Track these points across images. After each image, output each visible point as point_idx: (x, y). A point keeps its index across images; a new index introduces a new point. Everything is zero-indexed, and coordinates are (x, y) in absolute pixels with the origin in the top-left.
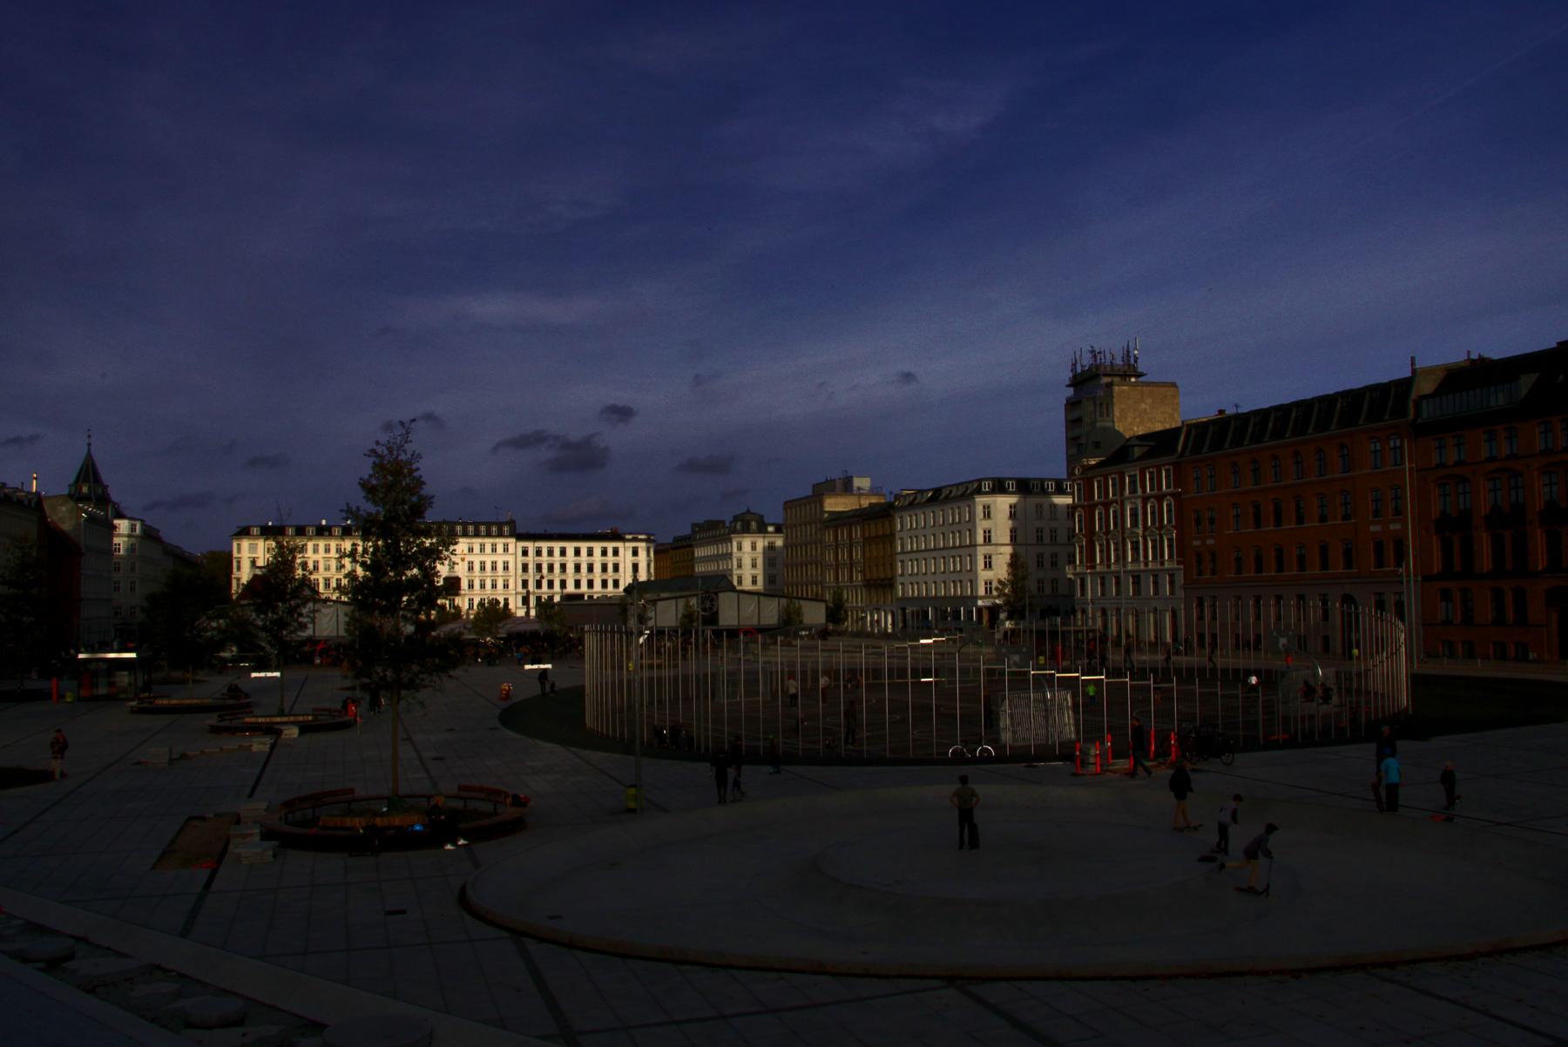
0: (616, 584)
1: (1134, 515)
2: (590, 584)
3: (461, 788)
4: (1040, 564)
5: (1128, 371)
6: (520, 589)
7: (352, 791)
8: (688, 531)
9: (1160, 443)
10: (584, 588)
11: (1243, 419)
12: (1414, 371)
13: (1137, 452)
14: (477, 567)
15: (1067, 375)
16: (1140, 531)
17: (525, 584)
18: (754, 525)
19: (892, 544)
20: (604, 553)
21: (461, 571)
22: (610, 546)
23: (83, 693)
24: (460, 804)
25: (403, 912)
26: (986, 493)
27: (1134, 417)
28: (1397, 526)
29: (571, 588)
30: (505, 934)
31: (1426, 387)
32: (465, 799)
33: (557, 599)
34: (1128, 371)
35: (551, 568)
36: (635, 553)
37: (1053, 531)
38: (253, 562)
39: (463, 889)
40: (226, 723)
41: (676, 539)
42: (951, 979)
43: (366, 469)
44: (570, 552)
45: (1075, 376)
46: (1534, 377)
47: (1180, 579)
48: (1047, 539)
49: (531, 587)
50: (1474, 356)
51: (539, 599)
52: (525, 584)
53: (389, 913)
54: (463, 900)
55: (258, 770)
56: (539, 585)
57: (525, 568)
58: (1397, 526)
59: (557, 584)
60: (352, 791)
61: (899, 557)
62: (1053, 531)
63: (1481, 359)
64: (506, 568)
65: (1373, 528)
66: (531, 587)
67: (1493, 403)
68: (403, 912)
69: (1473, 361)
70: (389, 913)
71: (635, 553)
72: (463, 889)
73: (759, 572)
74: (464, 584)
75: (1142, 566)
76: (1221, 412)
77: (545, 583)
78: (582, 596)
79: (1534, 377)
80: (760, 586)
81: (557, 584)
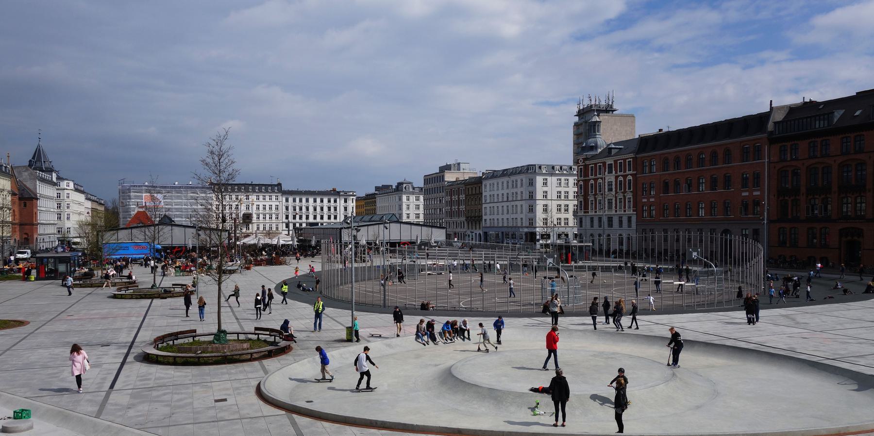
0: (335, 218)
2: (322, 218)
3: (256, 329)
4: (559, 210)
5: (608, 110)
6: (284, 220)
7: (195, 331)
8: (372, 191)
10: (318, 220)
11: (669, 135)
12: (771, 108)
14: (261, 208)
15: (575, 110)
19: (480, 199)
21: (253, 210)
24: (255, 337)
27: (609, 134)
28: (758, 193)
29: (311, 220)
31: (779, 117)
32: (258, 334)
34: (608, 110)
35: (301, 209)
40: (123, 292)
41: (367, 195)
43: (204, 155)
45: (579, 111)
46: (842, 112)
47: (634, 219)
49: (291, 219)
50: (807, 100)
51: (294, 225)
52: (287, 217)
53: (216, 401)
54: (260, 393)
55: (142, 319)
56: (294, 218)
58: (758, 193)
59: (304, 217)
60: (195, 331)
61: (484, 206)
63: (811, 102)
64: (277, 209)
65: (744, 194)
66: (291, 219)
67: (817, 126)
68: (225, 400)
69: (806, 103)
70: (216, 401)
72: (259, 385)
73: (421, 211)
74: (255, 216)
75: (614, 212)
76: (660, 130)
77: (298, 217)
78: (317, 224)
79: (842, 112)
80: (421, 219)
81: (304, 217)
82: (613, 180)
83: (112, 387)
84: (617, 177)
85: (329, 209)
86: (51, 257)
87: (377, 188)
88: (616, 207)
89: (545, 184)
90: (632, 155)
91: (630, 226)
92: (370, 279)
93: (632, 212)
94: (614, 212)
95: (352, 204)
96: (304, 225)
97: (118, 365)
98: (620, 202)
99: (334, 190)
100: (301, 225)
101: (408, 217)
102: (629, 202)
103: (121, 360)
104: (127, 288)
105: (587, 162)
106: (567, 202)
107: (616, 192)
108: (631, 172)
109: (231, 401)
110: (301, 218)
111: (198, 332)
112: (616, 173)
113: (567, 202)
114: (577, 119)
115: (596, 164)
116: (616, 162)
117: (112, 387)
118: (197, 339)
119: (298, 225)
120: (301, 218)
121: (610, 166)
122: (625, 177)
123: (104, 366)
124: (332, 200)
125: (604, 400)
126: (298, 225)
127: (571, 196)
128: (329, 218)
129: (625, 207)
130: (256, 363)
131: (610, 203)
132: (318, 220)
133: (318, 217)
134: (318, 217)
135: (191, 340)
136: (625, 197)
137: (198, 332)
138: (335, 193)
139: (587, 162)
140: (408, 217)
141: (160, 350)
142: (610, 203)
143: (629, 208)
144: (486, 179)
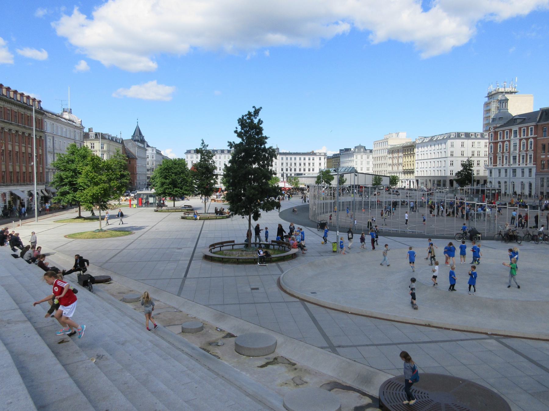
0: (313, 170)
1: (515, 146)
2: (304, 170)
7: (233, 242)
8: (338, 152)
9: (524, 119)
13: (518, 121)
16: (517, 151)
17: (282, 170)
18: (362, 150)
20: (309, 159)
22: (311, 157)
23: (436, 182)
25: (257, 289)
26: (453, 139)
29: (298, 172)
30: (298, 300)
33: (293, 175)
36: (320, 159)
37: (479, 152)
38: (192, 162)
39: (279, 280)
40: (187, 216)
41: (334, 155)
42: (492, 335)
44: (293, 159)
47: (534, 171)
48: (476, 155)
49: (284, 170)
51: (287, 175)
52: (282, 170)
57: (282, 164)
59: (293, 170)
62: (479, 152)
66: (284, 170)
71: (320, 159)
72: (279, 280)
75: (517, 166)
78: (301, 174)
81: (293, 170)
82: (518, 142)
83: (185, 276)
84: (520, 140)
85: (309, 164)
86: (144, 194)
87: (341, 150)
88: (519, 162)
89: (452, 146)
90: (534, 124)
91: (530, 176)
92: (343, 210)
93: (532, 165)
94: (517, 166)
95: (324, 161)
96: (293, 175)
97: (188, 262)
98: (523, 158)
99: (313, 152)
100: (291, 175)
101: (362, 170)
102: (531, 158)
103: (189, 259)
104: (189, 213)
105: (497, 130)
106: (479, 159)
107: (520, 151)
108: (533, 136)
109: (261, 290)
110: (291, 170)
111: (236, 242)
112: (520, 136)
113: (479, 159)
114: (486, 100)
115: (503, 131)
116: (520, 129)
117: (185, 276)
118: (235, 247)
119: (289, 175)
120: (291, 170)
121: (515, 132)
122: (527, 139)
123: (180, 262)
124: (289, 159)
125: (26, 321)
126: (289, 175)
127: (482, 154)
128: (309, 170)
129: (526, 161)
130: (274, 264)
131: (515, 158)
132: (302, 172)
133: (302, 170)
134: (302, 170)
135: (231, 247)
136: (527, 154)
137: (236, 242)
138: (313, 154)
139: (497, 130)
140: (362, 170)
141: (214, 253)
142: (515, 158)
143: (530, 162)
144: (423, 144)
